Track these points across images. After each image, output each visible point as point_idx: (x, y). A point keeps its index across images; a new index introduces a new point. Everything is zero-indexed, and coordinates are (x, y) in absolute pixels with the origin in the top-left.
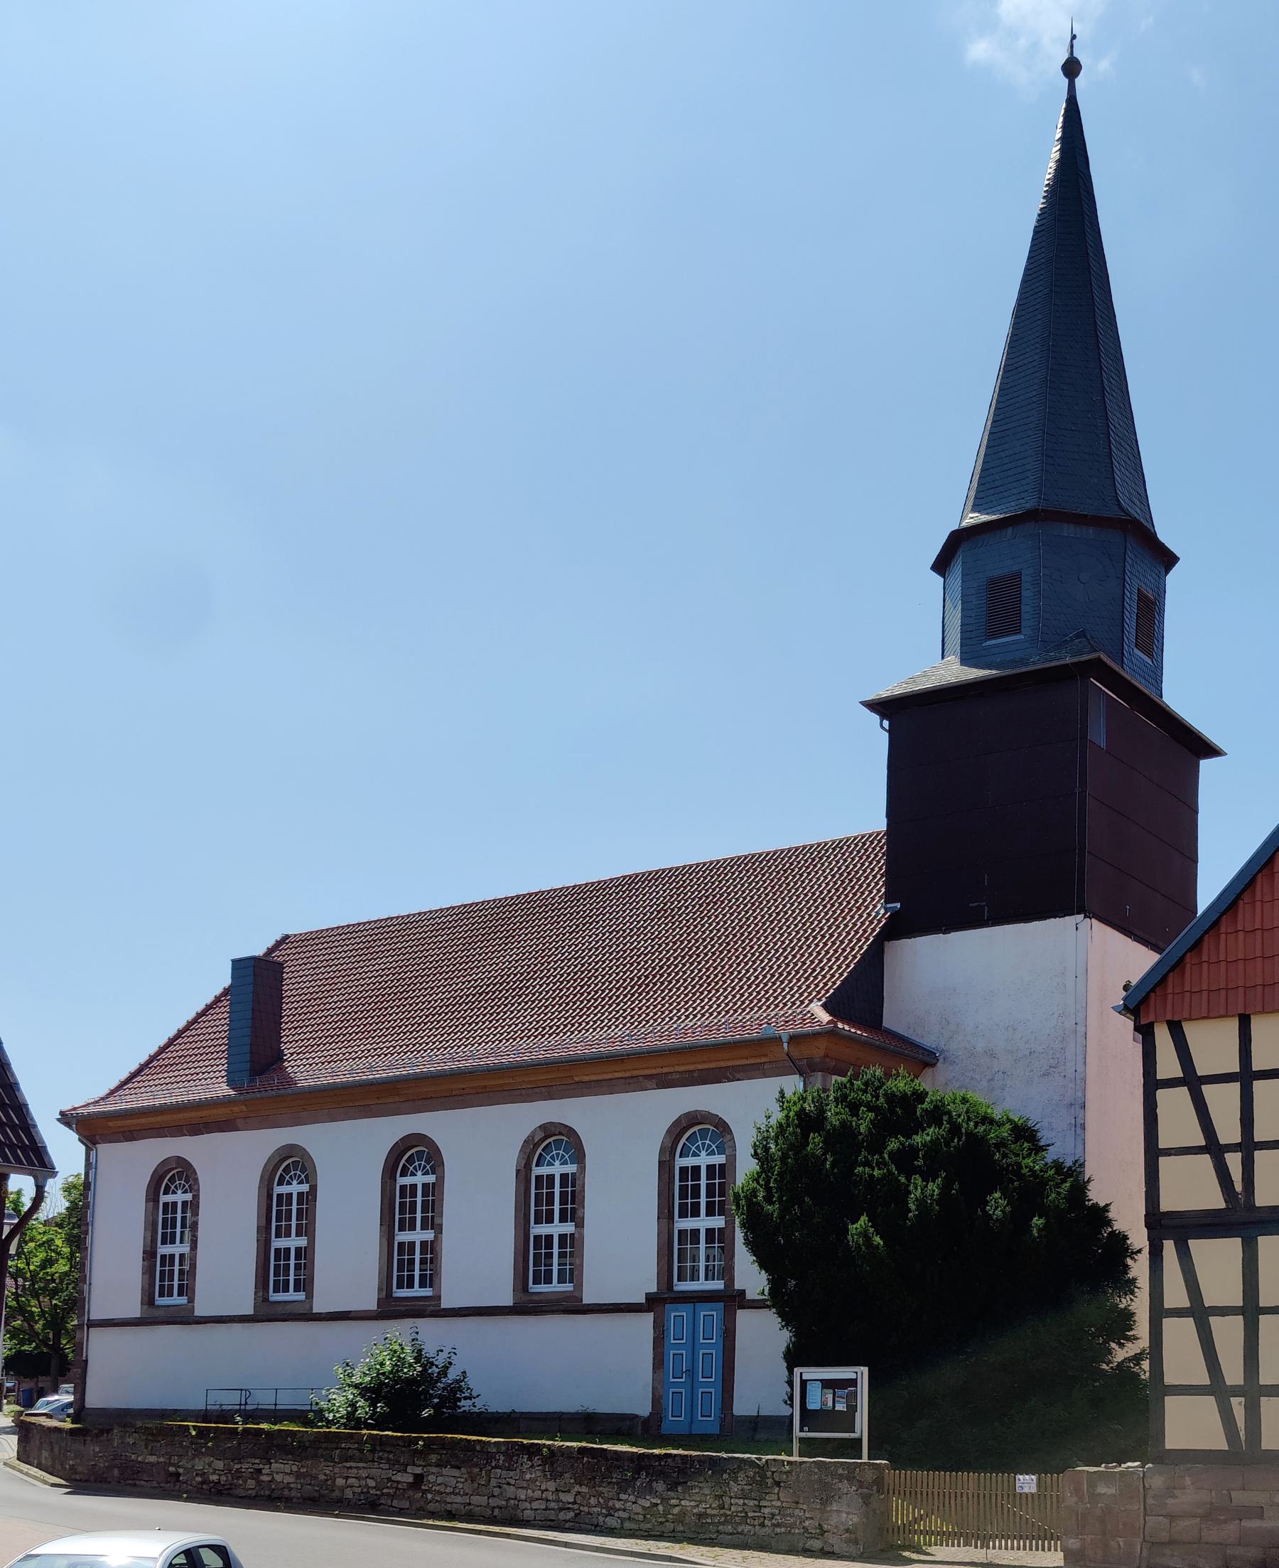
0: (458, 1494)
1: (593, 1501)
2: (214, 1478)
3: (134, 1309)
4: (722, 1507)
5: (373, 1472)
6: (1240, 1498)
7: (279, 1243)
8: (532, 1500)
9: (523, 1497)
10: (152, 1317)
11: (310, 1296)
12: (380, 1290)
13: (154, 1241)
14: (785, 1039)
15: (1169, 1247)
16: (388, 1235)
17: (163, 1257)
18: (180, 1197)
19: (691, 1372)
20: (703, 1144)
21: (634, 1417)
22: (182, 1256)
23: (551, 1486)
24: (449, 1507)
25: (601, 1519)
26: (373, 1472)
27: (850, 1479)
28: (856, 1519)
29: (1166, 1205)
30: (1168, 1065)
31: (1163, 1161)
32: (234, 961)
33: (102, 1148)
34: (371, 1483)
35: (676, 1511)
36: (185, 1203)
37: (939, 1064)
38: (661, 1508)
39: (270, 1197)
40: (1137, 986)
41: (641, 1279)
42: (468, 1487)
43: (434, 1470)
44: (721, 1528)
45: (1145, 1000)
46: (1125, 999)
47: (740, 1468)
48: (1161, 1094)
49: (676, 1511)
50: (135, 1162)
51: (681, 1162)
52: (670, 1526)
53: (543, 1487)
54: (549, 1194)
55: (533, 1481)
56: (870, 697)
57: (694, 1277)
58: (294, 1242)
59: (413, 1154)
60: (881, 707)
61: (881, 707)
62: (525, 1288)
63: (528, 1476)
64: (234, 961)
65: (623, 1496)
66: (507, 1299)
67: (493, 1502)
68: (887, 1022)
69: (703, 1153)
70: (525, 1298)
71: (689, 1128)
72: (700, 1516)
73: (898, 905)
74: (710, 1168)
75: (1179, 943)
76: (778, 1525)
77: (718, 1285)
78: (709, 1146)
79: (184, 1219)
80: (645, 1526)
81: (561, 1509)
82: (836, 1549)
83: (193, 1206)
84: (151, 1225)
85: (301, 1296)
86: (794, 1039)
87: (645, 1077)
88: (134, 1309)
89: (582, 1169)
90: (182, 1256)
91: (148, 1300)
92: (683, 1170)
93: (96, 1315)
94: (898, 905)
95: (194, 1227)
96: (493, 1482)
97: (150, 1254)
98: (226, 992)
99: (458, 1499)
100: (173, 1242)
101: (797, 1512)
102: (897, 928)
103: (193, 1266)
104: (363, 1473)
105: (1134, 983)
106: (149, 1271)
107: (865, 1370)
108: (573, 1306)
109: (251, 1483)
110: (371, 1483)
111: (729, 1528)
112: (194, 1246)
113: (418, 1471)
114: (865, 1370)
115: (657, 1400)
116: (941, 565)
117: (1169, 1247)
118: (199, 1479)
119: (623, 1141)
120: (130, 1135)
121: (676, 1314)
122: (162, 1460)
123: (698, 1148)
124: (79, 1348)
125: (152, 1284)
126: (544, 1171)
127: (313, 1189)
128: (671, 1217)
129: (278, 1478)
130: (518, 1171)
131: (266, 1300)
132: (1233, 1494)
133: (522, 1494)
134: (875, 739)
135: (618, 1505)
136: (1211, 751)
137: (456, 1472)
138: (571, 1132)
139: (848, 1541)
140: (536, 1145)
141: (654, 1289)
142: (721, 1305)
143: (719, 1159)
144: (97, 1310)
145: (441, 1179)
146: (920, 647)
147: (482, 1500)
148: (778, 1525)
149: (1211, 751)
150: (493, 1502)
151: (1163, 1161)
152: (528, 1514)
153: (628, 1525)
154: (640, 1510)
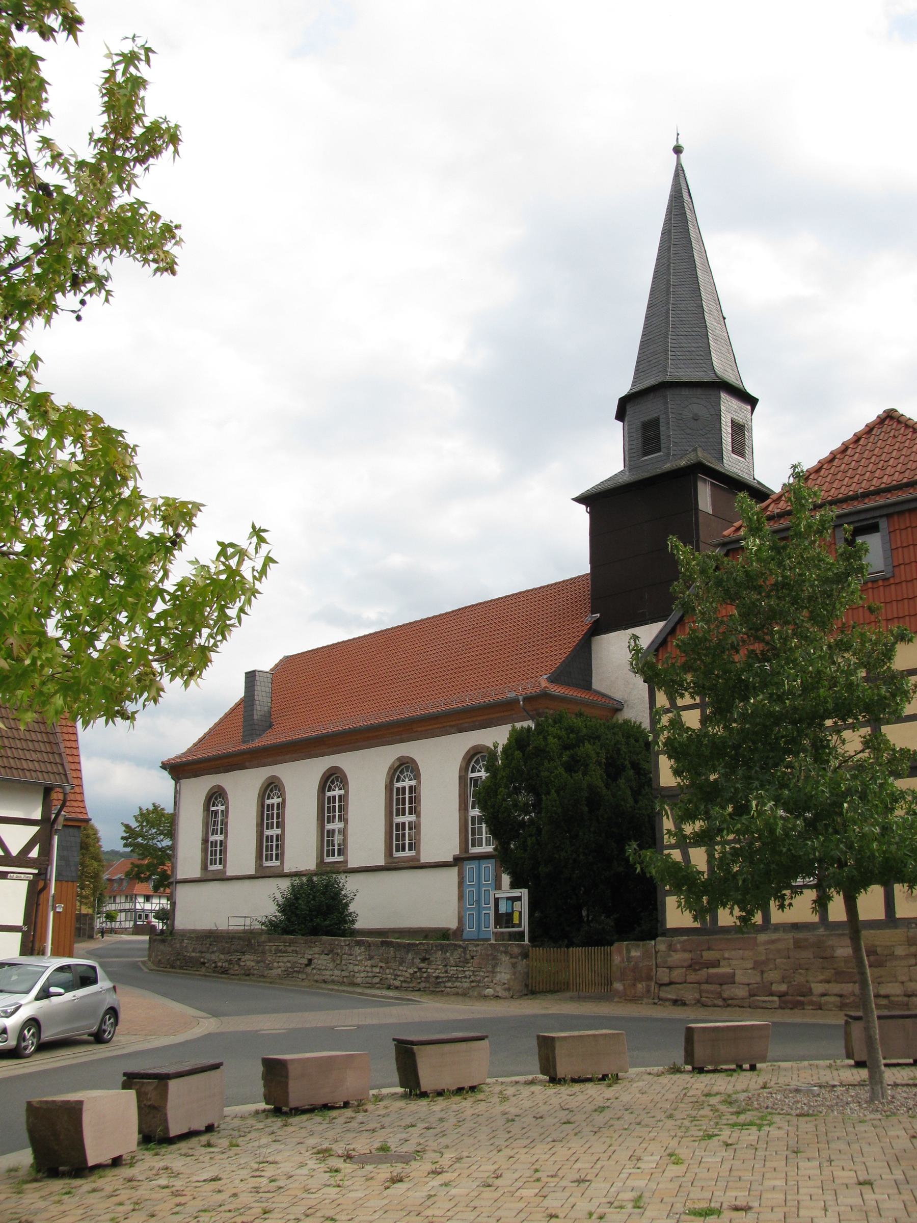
1: (388, 971)
2: (220, 964)
3: (197, 873)
4: (446, 972)
5: (290, 958)
6: (708, 955)
7: (268, 833)
10: (207, 878)
11: (282, 863)
12: (317, 858)
13: (207, 833)
14: (521, 698)
16: (321, 826)
19: (478, 902)
21: (448, 929)
24: (323, 978)
26: (290, 958)
27: (506, 953)
28: (508, 976)
32: (246, 673)
33: (184, 782)
35: (425, 975)
37: (625, 709)
39: (263, 806)
41: (449, 848)
42: (331, 966)
43: (317, 956)
47: (455, 949)
49: (425, 975)
50: (197, 789)
52: (423, 985)
54: (402, 799)
55: (361, 961)
58: (275, 832)
59: (333, 778)
62: (391, 854)
63: (359, 958)
64: (246, 673)
65: (401, 968)
66: (381, 861)
67: (344, 974)
68: (596, 685)
70: (391, 861)
72: (437, 977)
73: (598, 615)
75: (675, 616)
76: (472, 982)
80: (411, 985)
82: (500, 994)
84: (206, 825)
85: (278, 863)
86: (527, 699)
87: (451, 726)
88: (197, 873)
89: (419, 782)
91: (204, 867)
94: (598, 615)
96: (343, 962)
97: (205, 841)
99: (328, 973)
100: (404, 814)
102: (598, 629)
104: (285, 959)
106: (205, 851)
107: (526, 891)
108: (416, 865)
109: (236, 967)
110: (289, 965)
111: (449, 984)
112: (226, 837)
113: (310, 957)
114: (526, 891)
115: (461, 920)
119: (441, 763)
120: (196, 774)
121: (469, 866)
125: (206, 859)
126: (400, 785)
127: (284, 801)
128: (466, 809)
129: (248, 963)
130: (386, 786)
131: (261, 865)
132: (704, 953)
133: (356, 969)
134: (582, 516)
135: (399, 973)
137: (326, 957)
138: (413, 761)
139: (505, 989)
140: (396, 770)
141: (458, 853)
142: (493, 861)
144: (180, 875)
145: (347, 792)
146: (605, 456)
147: (337, 972)
150: (344, 974)
152: (359, 980)
153: (404, 985)
154: (408, 975)
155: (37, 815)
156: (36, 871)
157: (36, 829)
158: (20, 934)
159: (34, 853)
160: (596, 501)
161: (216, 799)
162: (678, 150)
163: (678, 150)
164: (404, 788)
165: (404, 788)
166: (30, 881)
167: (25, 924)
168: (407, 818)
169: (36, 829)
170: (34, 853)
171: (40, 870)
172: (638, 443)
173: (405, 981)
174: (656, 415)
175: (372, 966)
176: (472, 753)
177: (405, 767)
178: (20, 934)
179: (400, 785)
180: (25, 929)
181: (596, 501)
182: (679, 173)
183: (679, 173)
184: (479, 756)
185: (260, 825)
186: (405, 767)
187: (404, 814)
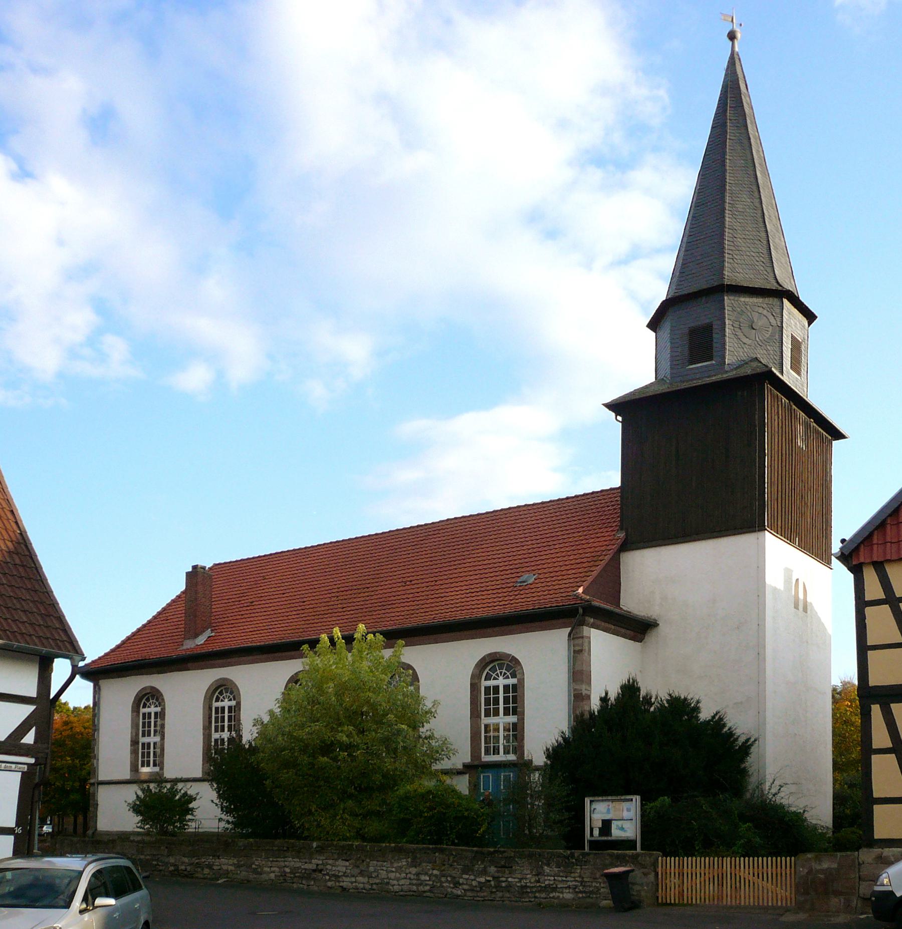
0: (347, 876)
2: (183, 867)
8: (398, 879)
9: (393, 877)
13: (137, 734)
15: (876, 710)
17: (143, 744)
18: (153, 710)
20: (501, 673)
22: (155, 744)
23: (414, 870)
24: (341, 884)
25: (449, 890)
29: (872, 682)
30: (874, 590)
31: (870, 653)
34: (288, 870)
35: (503, 884)
36: (156, 714)
38: (492, 883)
39: (210, 709)
40: (851, 540)
44: (537, 894)
45: (857, 549)
46: (841, 549)
48: (868, 610)
49: (503, 884)
50: (122, 694)
51: (485, 683)
53: (408, 871)
56: (608, 400)
57: (496, 751)
60: (616, 407)
61: (616, 407)
69: (501, 678)
71: (493, 663)
72: (522, 887)
74: (506, 688)
77: (512, 757)
78: (505, 674)
79: (155, 722)
81: (421, 884)
83: (161, 715)
84: (135, 725)
90: (155, 744)
91: (135, 769)
92: (487, 689)
93: (101, 778)
95: (163, 726)
97: (135, 742)
98: (183, 593)
100: (149, 735)
101: (594, 884)
102: (627, 546)
103: (163, 750)
105: (612, 696)
106: (134, 752)
112: (163, 738)
116: (654, 325)
117: (876, 710)
118: (172, 868)
122: (148, 857)
123: (497, 675)
124: (94, 795)
127: (239, 704)
134: (614, 426)
136: (838, 435)
138: (158, 691)
143: (512, 681)
146: (636, 363)
148: (581, 892)
149: (838, 435)
151: (870, 653)
155: (32, 691)
156: (32, 761)
157: (31, 708)
158: (12, 837)
159: (29, 738)
160: (624, 407)
161: (148, 700)
162: (732, 36)
163: (732, 36)
164: (150, 714)
165: (150, 714)
166: (23, 773)
167: (17, 824)
168: (153, 739)
169: (31, 708)
170: (29, 738)
171: (36, 759)
172: (691, 350)
173: (472, 890)
174: (708, 321)
175: (418, 874)
176: (488, 660)
177: (223, 688)
178: (12, 837)
179: (220, 704)
180: (19, 831)
181: (624, 407)
182: (733, 61)
183: (733, 61)
184: (496, 663)
185: (207, 728)
186: (151, 696)
187: (149, 735)
